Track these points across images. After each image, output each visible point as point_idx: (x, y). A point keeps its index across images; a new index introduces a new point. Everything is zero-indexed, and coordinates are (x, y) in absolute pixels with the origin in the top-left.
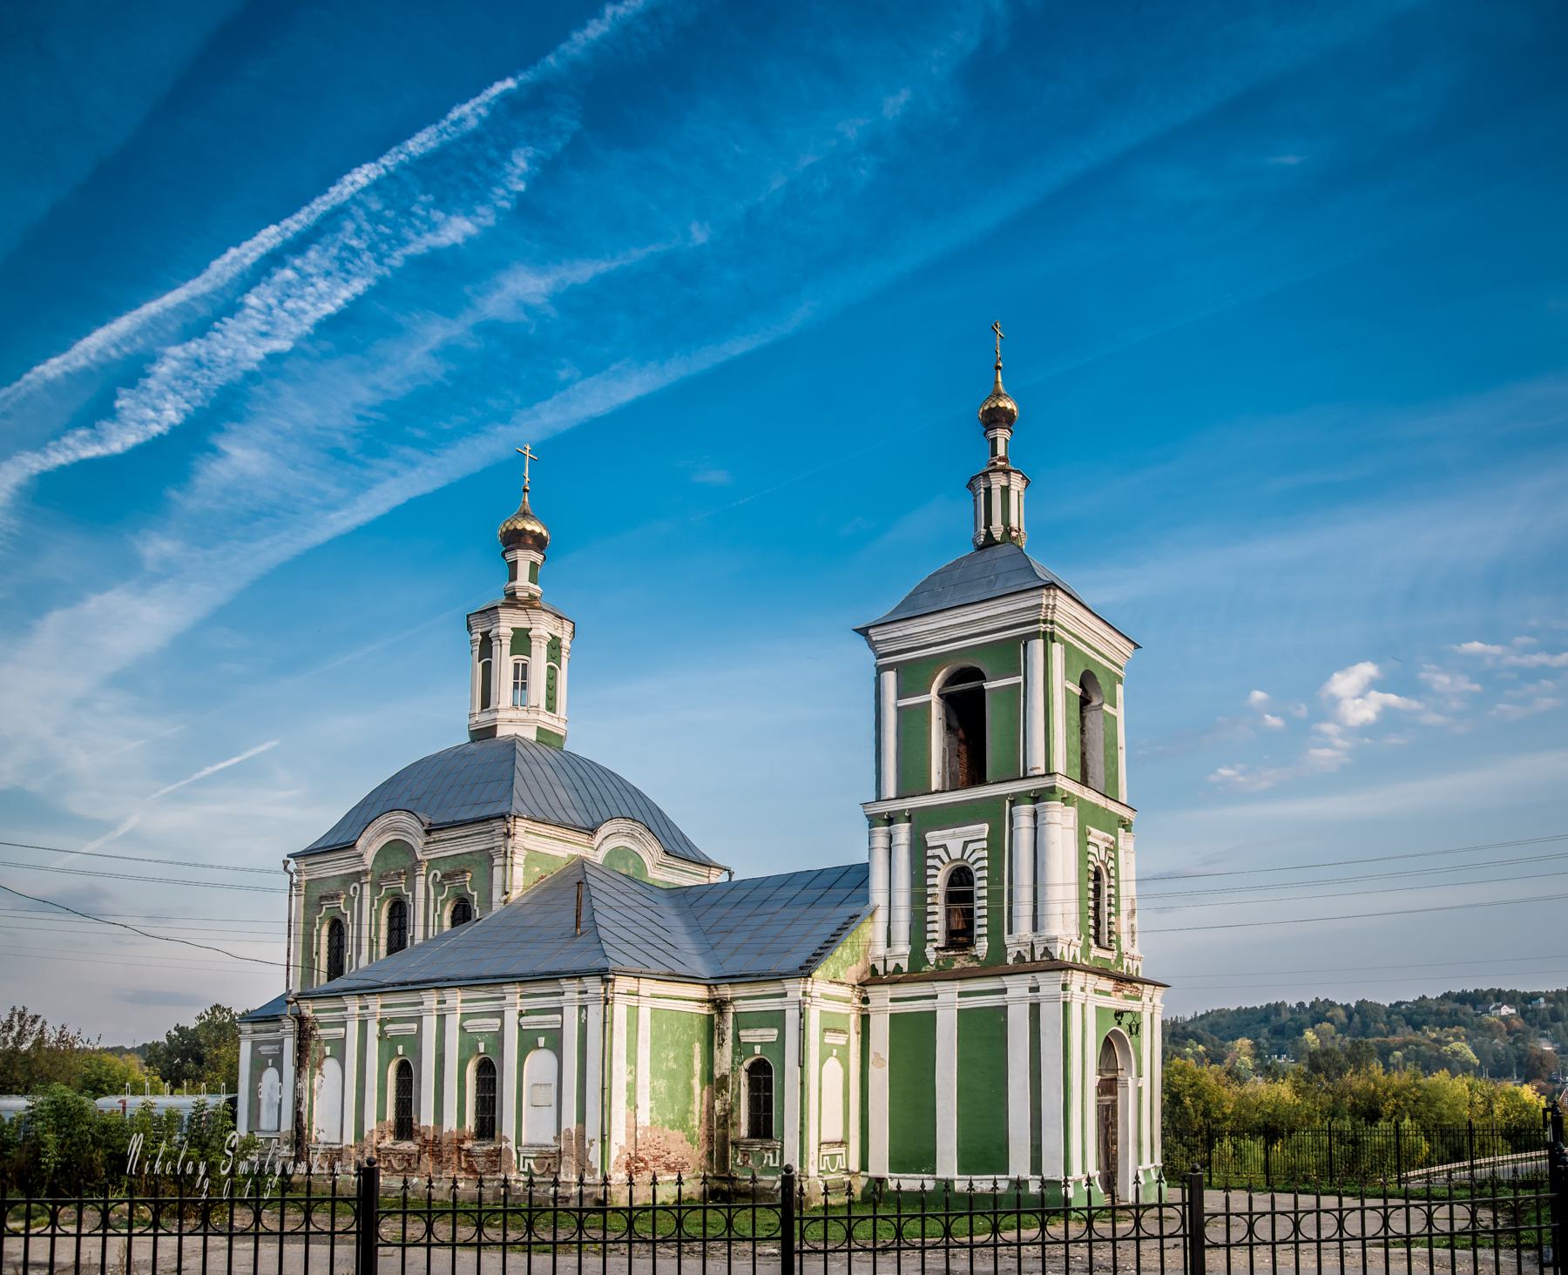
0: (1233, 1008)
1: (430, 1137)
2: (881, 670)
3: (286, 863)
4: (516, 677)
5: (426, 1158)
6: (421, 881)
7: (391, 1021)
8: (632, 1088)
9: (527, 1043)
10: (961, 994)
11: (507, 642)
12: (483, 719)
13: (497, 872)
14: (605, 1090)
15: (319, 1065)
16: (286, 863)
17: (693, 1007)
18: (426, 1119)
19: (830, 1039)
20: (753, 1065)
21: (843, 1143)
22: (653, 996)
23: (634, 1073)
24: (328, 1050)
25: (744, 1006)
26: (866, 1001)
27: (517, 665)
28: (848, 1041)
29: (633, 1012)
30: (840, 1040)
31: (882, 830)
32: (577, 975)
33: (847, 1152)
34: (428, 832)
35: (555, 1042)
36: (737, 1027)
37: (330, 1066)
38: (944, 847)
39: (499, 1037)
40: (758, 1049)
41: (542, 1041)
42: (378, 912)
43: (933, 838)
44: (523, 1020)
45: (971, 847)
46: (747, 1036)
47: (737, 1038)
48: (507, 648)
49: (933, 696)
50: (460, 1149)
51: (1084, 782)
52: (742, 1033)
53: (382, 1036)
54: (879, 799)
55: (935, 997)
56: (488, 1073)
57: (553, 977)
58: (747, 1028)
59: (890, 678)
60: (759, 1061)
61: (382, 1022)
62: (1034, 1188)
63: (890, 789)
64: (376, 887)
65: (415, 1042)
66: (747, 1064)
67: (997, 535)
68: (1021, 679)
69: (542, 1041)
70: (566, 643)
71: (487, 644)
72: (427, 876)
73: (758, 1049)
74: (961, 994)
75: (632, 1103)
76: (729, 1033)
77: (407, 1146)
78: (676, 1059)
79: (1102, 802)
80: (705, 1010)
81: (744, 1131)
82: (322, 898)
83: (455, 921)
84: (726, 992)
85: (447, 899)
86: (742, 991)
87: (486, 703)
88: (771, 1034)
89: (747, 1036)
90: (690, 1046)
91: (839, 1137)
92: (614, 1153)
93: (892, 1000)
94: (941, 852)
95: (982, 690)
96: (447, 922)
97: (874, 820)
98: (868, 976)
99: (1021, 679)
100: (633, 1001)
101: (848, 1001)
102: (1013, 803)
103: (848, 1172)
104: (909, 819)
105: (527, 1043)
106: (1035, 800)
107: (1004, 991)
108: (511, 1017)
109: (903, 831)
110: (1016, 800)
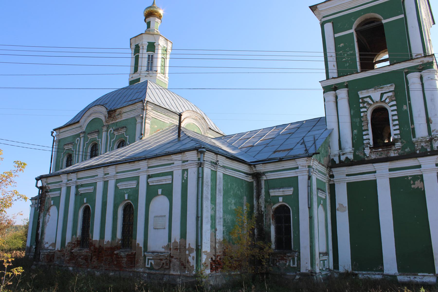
1: (97, 246)
2: (322, 25)
3: (52, 133)
5: (94, 259)
6: (104, 134)
8: (213, 218)
9: (151, 193)
10: (390, 170)
11: (145, 47)
12: (136, 76)
13: (138, 126)
14: (199, 218)
15: (48, 210)
16: (52, 133)
17: (242, 176)
18: (96, 236)
20: (277, 208)
21: (327, 254)
23: (214, 209)
24: (52, 202)
25: (271, 176)
26: (332, 176)
27: (149, 56)
28: (326, 197)
29: (214, 174)
31: (331, 94)
33: (328, 258)
35: (168, 191)
37: (53, 210)
38: (370, 97)
39: (136, 191)
40: (281, 199)
41: (160, 191)
42: (87, 148)
43: (362, 94)
44: (149, 180)
45: (385, 96)
46: (273, 193)
47: (267, 193)
49: (352, 31)
52: (271, 191)
53: (77, 194)
54: (328, 78)
55: (375, 172)
56: (130, 212)
58: (274, 188)
59: (329, 27)
60: (281, 206)
61: (77, 187)
63: (333, 72)
64: (85, 139)
65: (91, 197)
69: (160, 191)
70: (169, 51)
71: (137, 49)
72: (107, 131)
73: (281, 199)
74: (390, 170)
75: (213, 227)
77: (85, 251)
78: (235, 204)
79: (143, 251)
80: (249, 179)
84: (260, 168)
85: (115, 140)
87: (136, 70)
88: (289, 191)
90: (241, 198)
92: (204, 258)
93: (348, 175)
94: (368, 100)
97: (326, 89)
98: (330, 164)
102: (407, 73)
103: (330, 270)
104: (347, 87)
105: (151, 193)
106: (420, 70)
109: (343, 94)
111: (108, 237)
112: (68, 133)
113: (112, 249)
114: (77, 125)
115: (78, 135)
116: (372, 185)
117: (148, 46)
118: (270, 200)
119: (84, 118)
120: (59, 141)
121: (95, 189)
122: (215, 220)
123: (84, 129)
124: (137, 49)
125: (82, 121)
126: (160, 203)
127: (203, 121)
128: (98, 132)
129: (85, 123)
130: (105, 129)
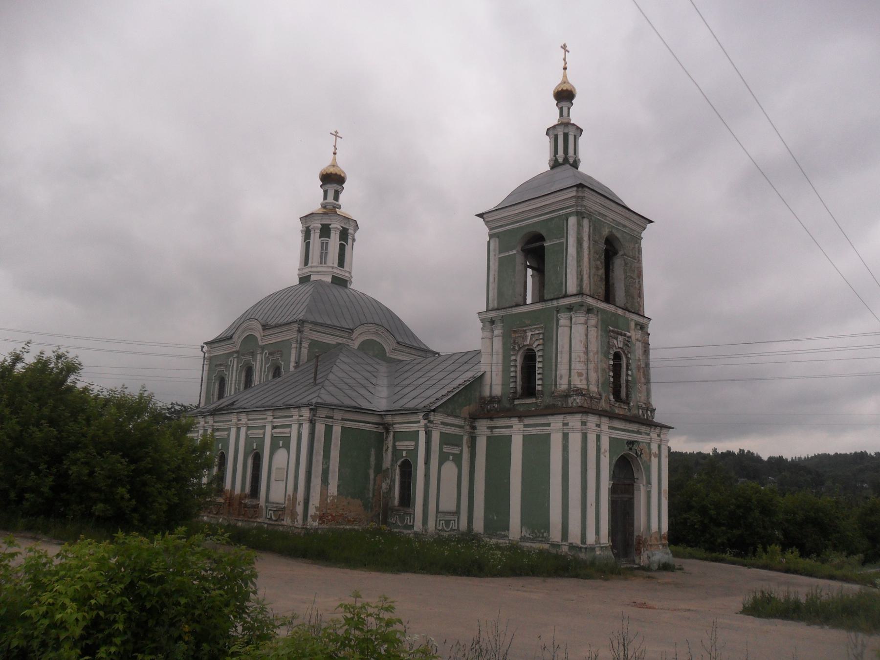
0: (832, 453)
1: (228, 495)
3: (203, 347)
4: (322, 249)
6: (259, 357)
7: (218, 430)
12: (307, 270)
16: (203, 347)
18: (228, 486)
19: (446, 449)
20: (403, 462)
22: (343, 419)
26: (474, 428)
27: (323, 243)
28: (461, 451)
30: (456, 451)
32: (299, 407)
34: (264, 330)
36: (395, 440)
40: (404, 453)
41: (451, 458)
44: (274, 431)
46: (401, 445)
48: (318, 235)
50: (241, 503)
51: (608, 297)
52: (397, 444)
56: (258, 459)
57: (288, 407)
62: (565, 549)
66: (399, 463)
67: (561, 160)
68: (564, 240)
69: (451, 458)
73: (404, 453)
75: (325, 481)
76: (390, 444)
81: (396, 502)
82: (216, 365)
83: (274, 377)
84: (389, 419)
86: (398, 419)
89: (401, 445)
91: (453, 508)
95: (543, 247)
96: (270, 377)
99: (564, 240)
100: (330, 422)
101: (461, 427)
102: (558, 312)
107: (549, 425)
108: (268, 428)
110: (558, 310)
111: (591, 539)
112: (220, 351)
113: (242, 497)
114: (230, 342)
115: (230, 354)
116: (507, 441)
117: (321, 230)
118: (396, 452)
119: (238, 332)
120: (210, 359)
121: (229, 435)
122: (328, 473)
123: (237, 348)
124: (307, 234)
125: (235, 337)
126: (281, 456)
127: (387, 334)
128: (253, 354)
129: (238, 340)
130: (259, 351)
